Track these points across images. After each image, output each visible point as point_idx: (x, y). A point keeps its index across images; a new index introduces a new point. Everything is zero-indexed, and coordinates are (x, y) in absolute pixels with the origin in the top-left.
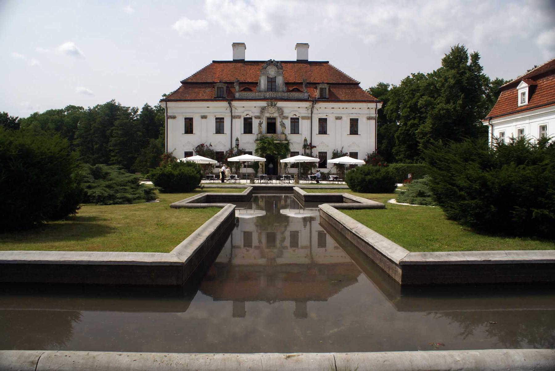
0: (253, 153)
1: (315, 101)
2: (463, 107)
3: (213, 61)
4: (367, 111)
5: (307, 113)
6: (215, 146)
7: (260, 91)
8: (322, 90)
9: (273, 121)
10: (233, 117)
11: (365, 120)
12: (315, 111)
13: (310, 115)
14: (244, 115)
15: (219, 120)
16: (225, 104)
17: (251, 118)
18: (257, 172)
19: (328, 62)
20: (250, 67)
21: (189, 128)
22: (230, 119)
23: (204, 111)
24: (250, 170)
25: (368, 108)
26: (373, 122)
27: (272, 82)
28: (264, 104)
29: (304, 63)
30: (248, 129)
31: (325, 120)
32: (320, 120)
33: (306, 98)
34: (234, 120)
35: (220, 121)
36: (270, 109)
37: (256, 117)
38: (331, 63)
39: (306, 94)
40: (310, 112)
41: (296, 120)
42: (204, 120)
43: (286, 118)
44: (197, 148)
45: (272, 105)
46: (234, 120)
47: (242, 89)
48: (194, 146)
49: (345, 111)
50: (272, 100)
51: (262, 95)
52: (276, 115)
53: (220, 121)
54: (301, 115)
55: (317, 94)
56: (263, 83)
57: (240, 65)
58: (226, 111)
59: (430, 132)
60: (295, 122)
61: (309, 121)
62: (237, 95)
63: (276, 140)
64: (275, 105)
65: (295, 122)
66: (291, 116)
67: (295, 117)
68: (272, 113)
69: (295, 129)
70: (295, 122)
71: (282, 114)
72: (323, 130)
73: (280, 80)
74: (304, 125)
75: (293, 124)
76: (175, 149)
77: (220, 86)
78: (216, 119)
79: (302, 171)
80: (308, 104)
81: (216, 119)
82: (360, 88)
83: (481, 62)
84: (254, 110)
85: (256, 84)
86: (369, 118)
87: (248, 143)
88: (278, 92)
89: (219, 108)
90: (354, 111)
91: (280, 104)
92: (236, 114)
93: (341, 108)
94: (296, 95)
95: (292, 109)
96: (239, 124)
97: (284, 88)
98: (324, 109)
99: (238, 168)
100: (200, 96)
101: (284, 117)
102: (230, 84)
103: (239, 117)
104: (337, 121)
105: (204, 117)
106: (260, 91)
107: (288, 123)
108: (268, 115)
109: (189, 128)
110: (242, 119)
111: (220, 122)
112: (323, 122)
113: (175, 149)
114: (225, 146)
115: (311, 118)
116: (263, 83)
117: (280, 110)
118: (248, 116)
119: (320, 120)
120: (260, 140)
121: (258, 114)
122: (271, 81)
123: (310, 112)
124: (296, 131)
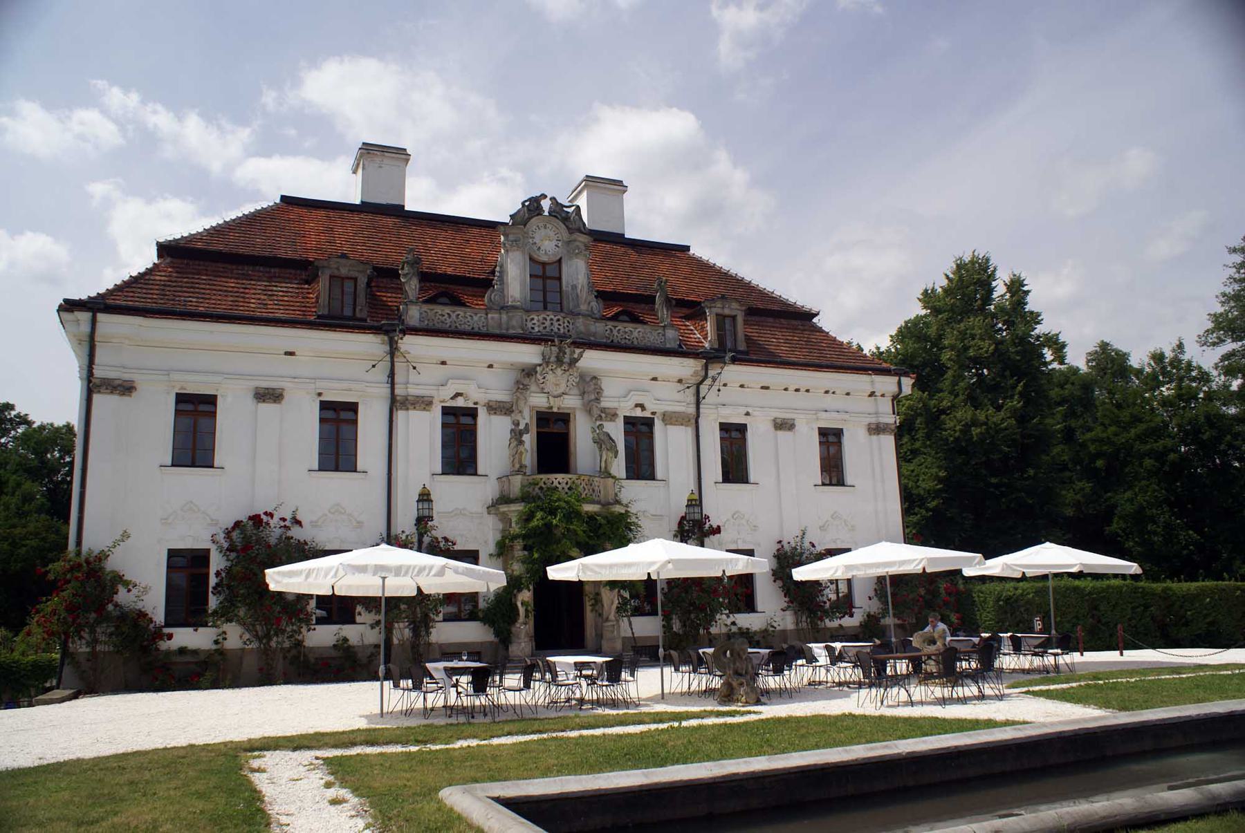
0: (482, 556)
1: (713, 357)
2: (1022, 418)
3: (283, 198)
4: (868, 405)
5: (682, 403)
6: (314, 524)
7: (504, 308)
8: (721, 320)
9: (557, 428)
10: (396, 403)
11: (862, 433)
12: (710, 397)
13: (692, 410)
14: (443, 396)
15: (330, 414)
16: (369, 344)
17: (472, 413)
18: (505, 639)
19: (688, 248)
20: (430, 231)
21: (195, 420)
22: (382, 409)
23: (273, 372)
24: (472, 632)
25: (872, 394)
26: (889, 441)
27: (544, 277)
28: (528, 354)
29: (616, 243)
30: (459, 452)
31: (742, 429)
32: (725, 428)
33: (672, 345)
34: (96, 398)
35: (338, 420)
36: (550, 377)
37: (496, 408)
38: (696, 251)
39: (671, 333)
40: (690, 396)
41: (344, 415)
42: (267, 408)
43: (613, 416)
44: (228, 533)
45: (559, 361)
46: (400, 415)
47: (432, 293)
48: (214, 523)
49: (801, 401)
50: (564, 345)
51: (515, 323)
52: (570, 402)
53: (338, 420)
54: (660, 408)
55: (706, 334)
56: (515, 278)
57: (390, 221)
58: (370, 376)
59: (937, 494)
60: (640, 431)
61: (689, 432)
62: (414, 314)
63: (593, 502)
64: (573, 362)
65: (338, 421)
66: (627, 409)
67: (638, 413)
68: (554, 391)
69: (641, 464)
70: (338, 421)
71: (598, 400)
72: (735, 469)
73: (577, 273)
74: (671, 446)
75: (187, 421)
76: (125, 536)
77: (344, 271)
78: (325, 406)
79: (676, 626)
80: (687, 368)
81: (325, 406)
82: (820, 330)
83: (1032, 304)
84: (488, 377)
85: (483, 283)
86: (876, 429)
87: (459, 513)
88: (574, 314)
89: (340, 361)
90: (829, 401)
91: (592, 360)
92: (413, 391)
93: (792, 388)
94: (636, 332)
95: (635, 380)
96: (422, 435)
97: (594, 304)
98: (745, 391)
99: (421, 624)
100: (253, 307)
101: (603, 410)
102: (386, 275)
103: (424, 403)
104: (780, 433)
105: (783, 425)
106: (504, 308)
107: (616, 430)
108: (539, 401)
109: (195, 420)
110: (436, 415)
111: (196, 413)
112: (734, 436)
113: (125, 536)
114: (360, 524)
115: (695, 422)
116: (515, 278)
117: (590, 386)
118: (460, 402)
119: (725, 428)
120: (525, 498)
121: (502, 396)
122: (545, 276)
123: (692, 399)
124: (644, 468)
